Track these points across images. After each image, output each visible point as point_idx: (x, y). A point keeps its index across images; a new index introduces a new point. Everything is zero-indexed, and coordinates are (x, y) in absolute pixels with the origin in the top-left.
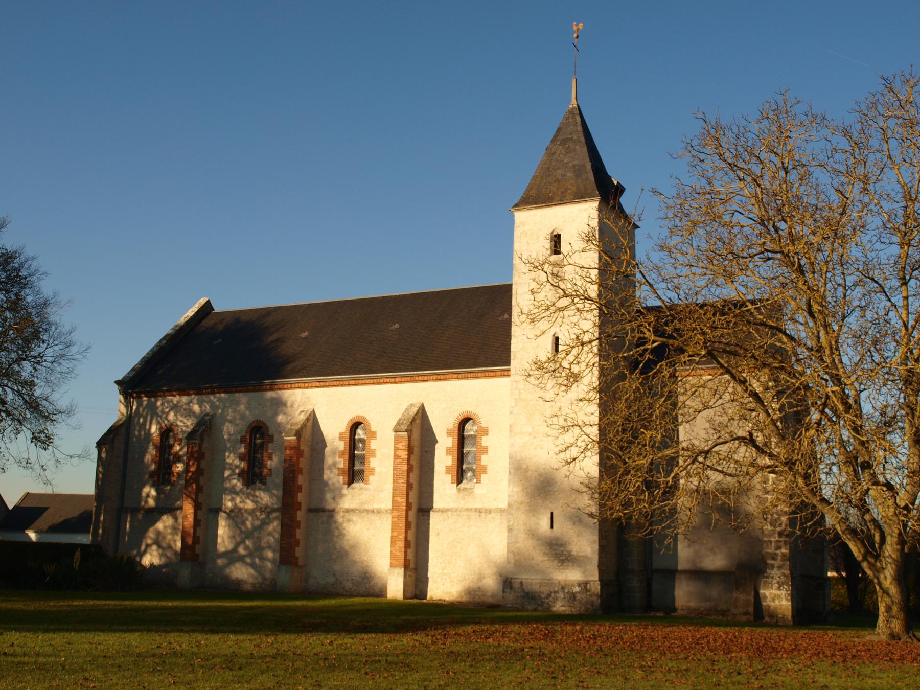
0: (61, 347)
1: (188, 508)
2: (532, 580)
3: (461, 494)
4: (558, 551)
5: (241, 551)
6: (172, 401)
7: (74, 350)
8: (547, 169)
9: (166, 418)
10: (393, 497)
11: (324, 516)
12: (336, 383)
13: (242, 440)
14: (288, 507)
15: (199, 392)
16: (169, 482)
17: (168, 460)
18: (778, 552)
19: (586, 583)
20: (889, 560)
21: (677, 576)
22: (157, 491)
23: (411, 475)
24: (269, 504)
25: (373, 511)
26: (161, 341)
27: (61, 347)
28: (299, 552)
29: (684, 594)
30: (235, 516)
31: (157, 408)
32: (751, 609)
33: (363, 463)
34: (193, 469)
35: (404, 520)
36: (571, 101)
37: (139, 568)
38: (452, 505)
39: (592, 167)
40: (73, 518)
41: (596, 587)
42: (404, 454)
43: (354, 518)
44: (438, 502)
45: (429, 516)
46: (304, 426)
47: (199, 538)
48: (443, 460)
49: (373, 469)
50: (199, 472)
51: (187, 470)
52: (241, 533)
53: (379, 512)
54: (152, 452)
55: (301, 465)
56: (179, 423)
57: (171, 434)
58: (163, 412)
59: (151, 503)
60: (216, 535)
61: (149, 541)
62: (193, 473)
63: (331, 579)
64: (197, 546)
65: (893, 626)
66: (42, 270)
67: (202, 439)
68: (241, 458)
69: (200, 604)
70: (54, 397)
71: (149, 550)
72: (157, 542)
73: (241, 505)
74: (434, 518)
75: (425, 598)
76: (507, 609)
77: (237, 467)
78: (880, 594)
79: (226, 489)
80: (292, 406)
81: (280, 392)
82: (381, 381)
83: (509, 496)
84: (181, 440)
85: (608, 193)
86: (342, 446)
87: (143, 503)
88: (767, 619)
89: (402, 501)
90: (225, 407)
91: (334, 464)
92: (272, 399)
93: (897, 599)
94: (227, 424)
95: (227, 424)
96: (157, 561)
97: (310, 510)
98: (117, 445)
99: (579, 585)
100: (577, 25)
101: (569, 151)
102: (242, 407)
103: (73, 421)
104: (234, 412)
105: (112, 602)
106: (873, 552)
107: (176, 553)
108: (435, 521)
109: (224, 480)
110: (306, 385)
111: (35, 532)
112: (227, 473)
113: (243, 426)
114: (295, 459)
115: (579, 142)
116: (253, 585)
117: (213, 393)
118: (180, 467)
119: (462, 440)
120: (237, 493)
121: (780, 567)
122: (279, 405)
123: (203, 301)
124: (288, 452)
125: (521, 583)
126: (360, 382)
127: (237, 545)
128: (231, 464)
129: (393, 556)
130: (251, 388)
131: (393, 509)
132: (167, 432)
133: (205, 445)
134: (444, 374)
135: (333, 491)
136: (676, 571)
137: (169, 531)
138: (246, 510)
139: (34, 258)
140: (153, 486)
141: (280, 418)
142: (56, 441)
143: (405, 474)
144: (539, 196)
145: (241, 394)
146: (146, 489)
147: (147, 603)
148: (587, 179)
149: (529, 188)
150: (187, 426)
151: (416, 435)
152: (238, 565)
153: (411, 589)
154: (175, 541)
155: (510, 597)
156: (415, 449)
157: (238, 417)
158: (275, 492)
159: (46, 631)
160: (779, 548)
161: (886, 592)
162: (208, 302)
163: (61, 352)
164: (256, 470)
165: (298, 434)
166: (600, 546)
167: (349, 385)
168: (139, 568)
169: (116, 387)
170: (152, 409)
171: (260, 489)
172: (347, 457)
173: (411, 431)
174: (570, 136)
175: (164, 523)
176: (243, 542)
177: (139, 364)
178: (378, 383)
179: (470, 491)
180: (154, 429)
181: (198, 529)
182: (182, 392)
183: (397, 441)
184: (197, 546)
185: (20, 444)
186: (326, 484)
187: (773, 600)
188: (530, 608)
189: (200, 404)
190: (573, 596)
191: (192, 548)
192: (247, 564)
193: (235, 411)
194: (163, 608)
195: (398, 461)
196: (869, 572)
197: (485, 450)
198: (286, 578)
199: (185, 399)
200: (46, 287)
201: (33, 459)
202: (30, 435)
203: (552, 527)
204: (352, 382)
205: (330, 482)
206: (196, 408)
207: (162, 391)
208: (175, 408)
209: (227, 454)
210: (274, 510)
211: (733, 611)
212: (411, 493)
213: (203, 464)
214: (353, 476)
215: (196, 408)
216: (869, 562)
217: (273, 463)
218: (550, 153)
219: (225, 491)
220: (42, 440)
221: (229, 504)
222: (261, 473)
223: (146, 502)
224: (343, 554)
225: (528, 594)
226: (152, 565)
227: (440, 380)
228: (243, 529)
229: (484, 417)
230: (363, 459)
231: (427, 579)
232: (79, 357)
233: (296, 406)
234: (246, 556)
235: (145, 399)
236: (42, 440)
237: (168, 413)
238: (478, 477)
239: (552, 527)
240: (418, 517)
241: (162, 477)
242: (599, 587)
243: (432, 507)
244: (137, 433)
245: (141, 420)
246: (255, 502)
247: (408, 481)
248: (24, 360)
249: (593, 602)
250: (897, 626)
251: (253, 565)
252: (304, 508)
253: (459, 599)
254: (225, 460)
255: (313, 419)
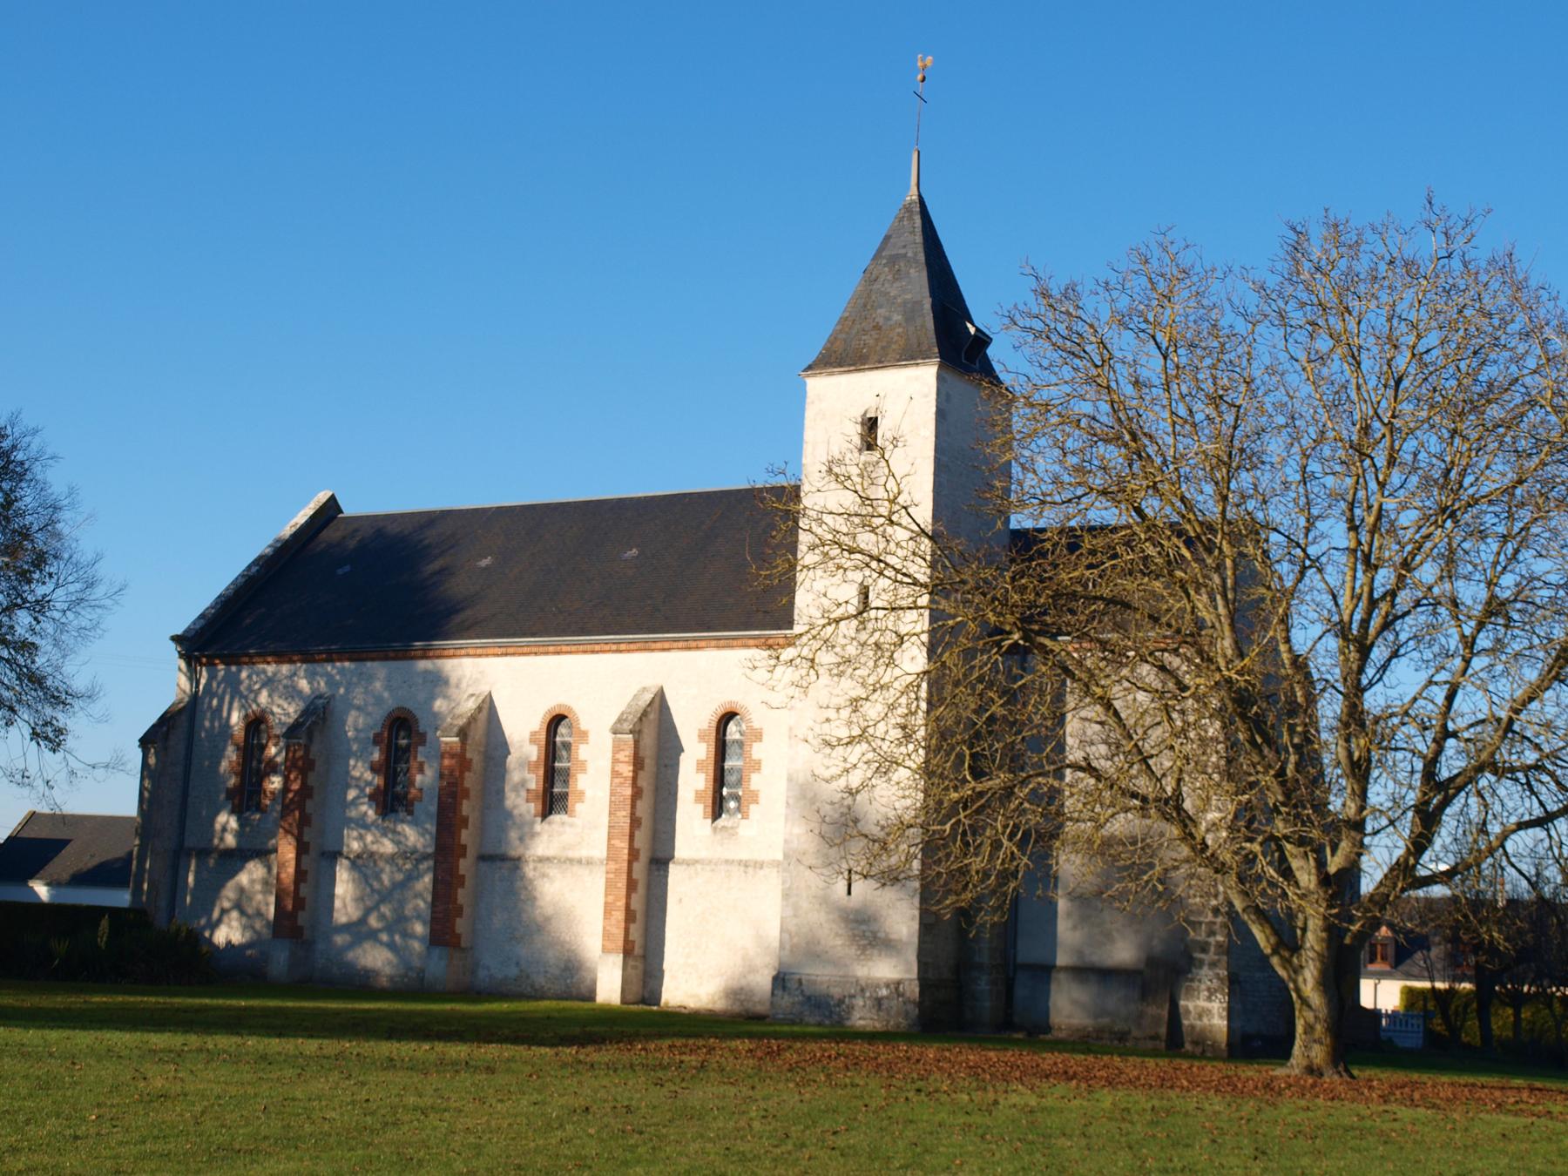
0: (78, 586)
1: (287, 850)
2: (821, 976)
3: (718, 837)
4: (865, 931)
5: (373, 922)
6: (264, 672)
7: (99, 591)
8: (863, 305)
9: (255, 701)
10: (609, 839)
11: (504, 865)
12: (525, 650)
13: (377, 740)
14: (446, 851)
15: (308, 658)
16: (259, 808)
17: (258, 770)
18: (1212, 940)
19: (898, 983)
20: (1311, 954)
21: (1054, 975)
22: (239, 820)
23: (639, 803)
24: (419, 846)
25: (580, 862)
26: (249, 567)
27: (78, 586)
28: (461, 925)
29: (1068, 1006)
30: (364, 865)
31: (240, 682)
32: (1163, 1031)
33: (566, 782)
34: (295, 786)
35: (624, 877)
36: (908, 188)
37: (205, 949)
38: (703, 854)
39: (934, 306)
40: (117, 860)
41: (913, 990)
42: (627, 770)
43: (553, 871)
44: (682, 849)
45: (667, 871)
46: (472, 719)
47: (303, 900)
48: (692, 779)
49: (582, 793)
50: (306, 792)
51: (286, 789)
52: (374, 895)
53: (589, 862)
54: (231, 755)
55: (467, 784)
56: (275, 709)
57: (263, 727)
58: (250, 689)
59: (230, 840)
60: (332, 896)
61: (226, 904)
62: (296, 792)
63: (513, 972)
64: (300, 913)
65: (1313, 1054)
66: (49, 451)
67: (310, 738)
68: (374, 769)
69: (290, 1004)
70: (69, 668)
71: (225, 919)
72: (238, 906)
73: (374, 848)
74: (675, 873)
75: (658, 1003)
76: (784, 1022)
77: (368, 784)
78: (1297, 1006)
79: (351, 820)
80: (457, 686)
81: (439, 662)
82: (597, 648)
83: (786, 841)
84: (277, 737)
85: (960, 350)
86: (534, 752)
87: (216, 841)
88: (1188, 1047)
89: (623, 845)
90: (349, 684)
91: (523, 783)
92: (427, 672)
93: (1323, 1013)
94: (353, 713)
95: (353, 713)
96: (237, 937)
97: (483, 858)
98: (172, 741)
99: (887, 986)
100: (923, 60)
101: (898, 276)
102: (378, 685)
103: (96, 708)
104: (364, 692)
105: (153, 999)
106: (1289, 943)
107: (268, 922)
108: (676, 876)
109: (346, 805)
110: (479, 651)
111: (47, 884)
112: (352, 794)
113: (379, 714)
114: (457, 774)
115: (917, 262)
116: (391, 978)
117: (330, 660)
118: (275, 783)
119: (721, 749)
120: (366, 827)
121: (1213, 965)
122: (438, 682)
123: (323, 497)
124: (447, 762)
125: (800, 982)
126: (564, 648)
127: (367, 912)
128: (358, 779)
129: (607, 935)
130: (392, 654)
131: (609, 858)
132: (256, 724)
133: (315, 748)
134: (695, 639)
135: (520, 827)
136: (1053, 967)
137: (258, 887)
138: (381, 855)
139: (35, 432)
140: (232, 812)
141: (439, 705)
142: (70, 742)
143: (629, 802)
144: (843, 355)
145: (376, 664)
146: (222, 818)
147: (207, 1001)
148: (923, 326)
149: (832, 340)
150: (288, 715)
151: (648, 740)
152: (367, 946)
153: (636, 989)
154: (267, 904)
155: (786, 1001)
156: (647, 761)
157: (371, 700)
158: (428, 826)
159: (39, 1028)
160: (1212, 933)
161: (1305, 1002)
162: (333, 499)
163: (79, 595)
164: (399, 788)
165: (463, 733)
166: (921, 923)
167: (547, 653)
168: (205, 949)
169: (173, 645)
170: (233, 683)
171: (403, 821)
172: (541, 772)
173: (640, 732)
174: (902, 251)
175: (251, 875)
176: (376, 907)
177: (211, 607)
178: (593, 652)
179: (731, 832)
180: (235, 717)
181: (302, 885)
182: (281, 657)
183: (617, 749)
184: (299, 914)
185: (10, 743)
186: (509, 815)
187: (1200, 1017)
188: (812, 1020)
189: (311, 677)
190: (879, 1002)
191: (293, 916)
192: (381, 943)
193: (366, 692)
194: (230, 1008)
195: (617, 780)
196: (1282, 972)
197: (757, 766)
198: (438, 967)
199: (285, 669)
200: (55, 478)
201: (32, 771)
202: (27, 731)
203: (849, 893)
204: (551, 649)
205: (516, 812)
206: (304, 684)
207: (248, 655)
208: (269, 683)
209: (352, 762)
210: (425, 857)
211: (1135, 1033)
212: (637, 833)
213: (312, 779)
214: (552, 803)
215: (304, 684)
216: (1282, 957)
217: (425, 778)
218: (870, 278)
219: (348, 822)
220: (50, 736)
221: (355, 846)
222: (407, 793)
223: (222, 839)
224: (539, 928)
225: (809, 998)
226: (229, 943)
227: (689, 649)
228: (376, 885)
229: (756, 714)
230: (566, 775)
231: (662, 972)
232: (108, 602)
233: (464, 685)
234: (380, 931)
235: (221, 667)
236: (50, 736)
237: (257, 693)
238: (725, 809)
239: (849, 893)
240: (650, 872)
241: (246, 798)
242: (917, 990)
243: (672, 857)
244: (207, 724)
245: (215, 702)
246: (397, 843)
247: (632, 814)
248: (20, 607)
249: (907, 1013)
250: (1319, 1054)
251: (391, 946)
252: (471, 853)
253: (710, 1006)
254: (348, 772)
255: (488, 709)
